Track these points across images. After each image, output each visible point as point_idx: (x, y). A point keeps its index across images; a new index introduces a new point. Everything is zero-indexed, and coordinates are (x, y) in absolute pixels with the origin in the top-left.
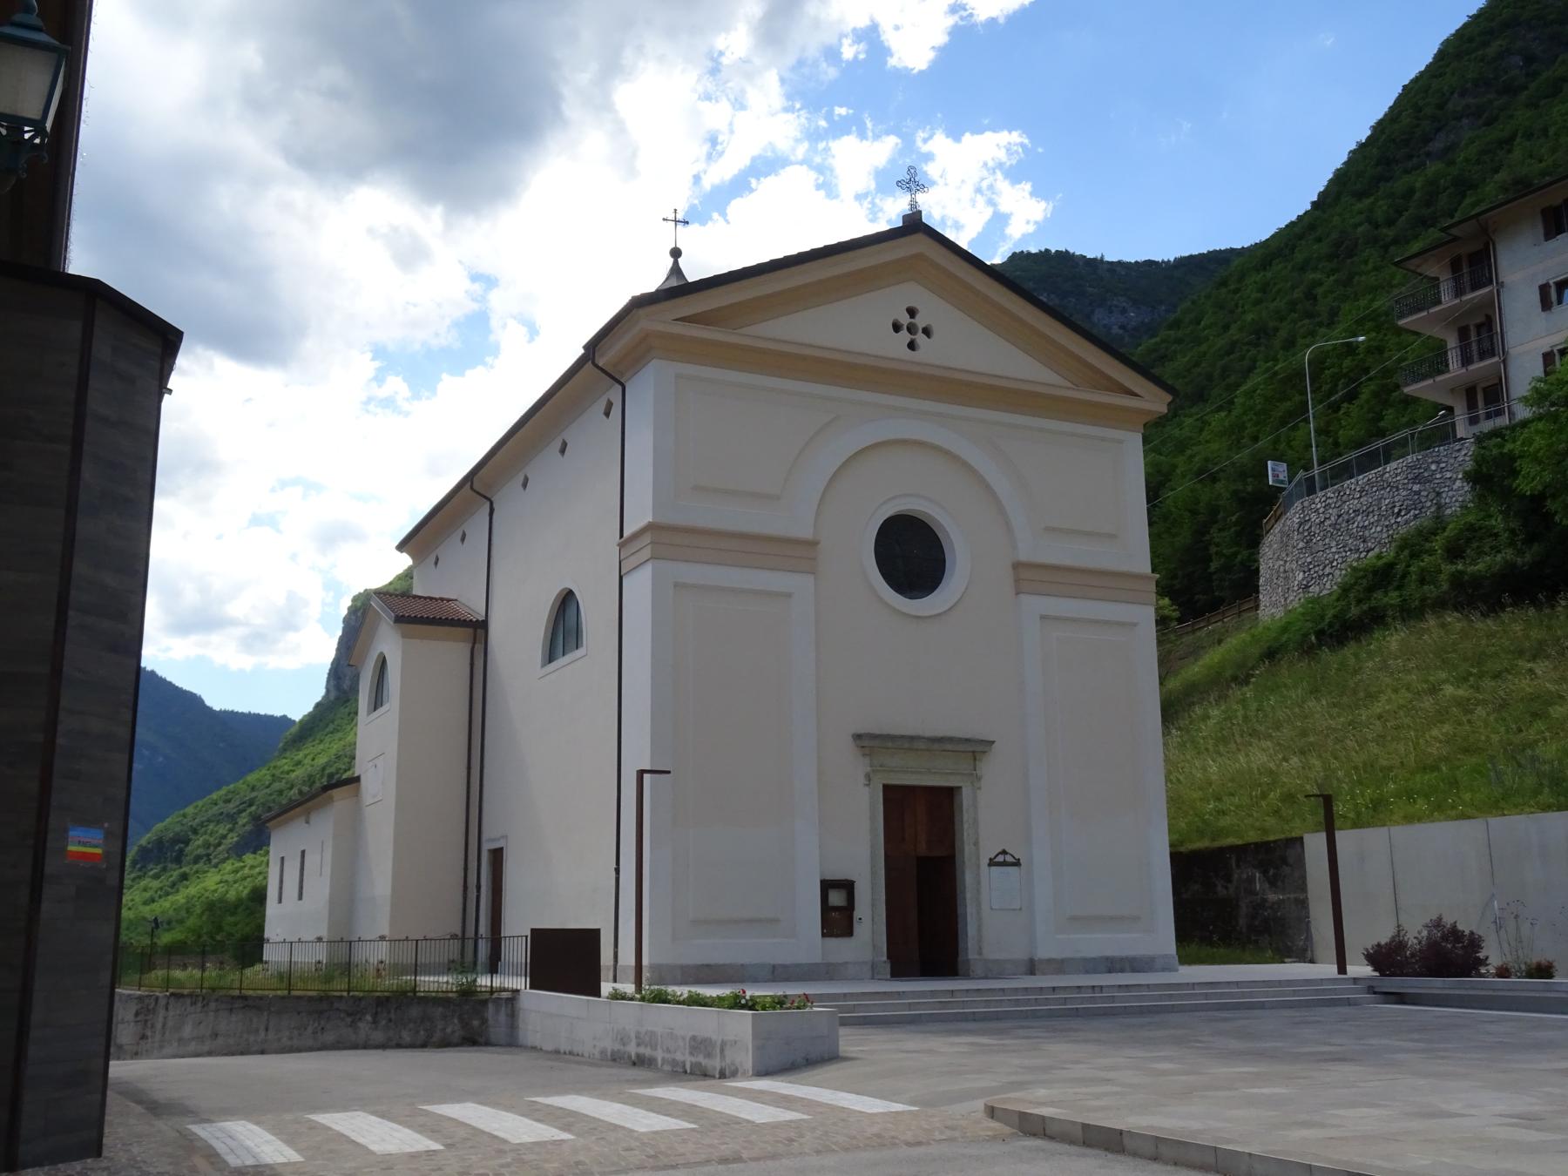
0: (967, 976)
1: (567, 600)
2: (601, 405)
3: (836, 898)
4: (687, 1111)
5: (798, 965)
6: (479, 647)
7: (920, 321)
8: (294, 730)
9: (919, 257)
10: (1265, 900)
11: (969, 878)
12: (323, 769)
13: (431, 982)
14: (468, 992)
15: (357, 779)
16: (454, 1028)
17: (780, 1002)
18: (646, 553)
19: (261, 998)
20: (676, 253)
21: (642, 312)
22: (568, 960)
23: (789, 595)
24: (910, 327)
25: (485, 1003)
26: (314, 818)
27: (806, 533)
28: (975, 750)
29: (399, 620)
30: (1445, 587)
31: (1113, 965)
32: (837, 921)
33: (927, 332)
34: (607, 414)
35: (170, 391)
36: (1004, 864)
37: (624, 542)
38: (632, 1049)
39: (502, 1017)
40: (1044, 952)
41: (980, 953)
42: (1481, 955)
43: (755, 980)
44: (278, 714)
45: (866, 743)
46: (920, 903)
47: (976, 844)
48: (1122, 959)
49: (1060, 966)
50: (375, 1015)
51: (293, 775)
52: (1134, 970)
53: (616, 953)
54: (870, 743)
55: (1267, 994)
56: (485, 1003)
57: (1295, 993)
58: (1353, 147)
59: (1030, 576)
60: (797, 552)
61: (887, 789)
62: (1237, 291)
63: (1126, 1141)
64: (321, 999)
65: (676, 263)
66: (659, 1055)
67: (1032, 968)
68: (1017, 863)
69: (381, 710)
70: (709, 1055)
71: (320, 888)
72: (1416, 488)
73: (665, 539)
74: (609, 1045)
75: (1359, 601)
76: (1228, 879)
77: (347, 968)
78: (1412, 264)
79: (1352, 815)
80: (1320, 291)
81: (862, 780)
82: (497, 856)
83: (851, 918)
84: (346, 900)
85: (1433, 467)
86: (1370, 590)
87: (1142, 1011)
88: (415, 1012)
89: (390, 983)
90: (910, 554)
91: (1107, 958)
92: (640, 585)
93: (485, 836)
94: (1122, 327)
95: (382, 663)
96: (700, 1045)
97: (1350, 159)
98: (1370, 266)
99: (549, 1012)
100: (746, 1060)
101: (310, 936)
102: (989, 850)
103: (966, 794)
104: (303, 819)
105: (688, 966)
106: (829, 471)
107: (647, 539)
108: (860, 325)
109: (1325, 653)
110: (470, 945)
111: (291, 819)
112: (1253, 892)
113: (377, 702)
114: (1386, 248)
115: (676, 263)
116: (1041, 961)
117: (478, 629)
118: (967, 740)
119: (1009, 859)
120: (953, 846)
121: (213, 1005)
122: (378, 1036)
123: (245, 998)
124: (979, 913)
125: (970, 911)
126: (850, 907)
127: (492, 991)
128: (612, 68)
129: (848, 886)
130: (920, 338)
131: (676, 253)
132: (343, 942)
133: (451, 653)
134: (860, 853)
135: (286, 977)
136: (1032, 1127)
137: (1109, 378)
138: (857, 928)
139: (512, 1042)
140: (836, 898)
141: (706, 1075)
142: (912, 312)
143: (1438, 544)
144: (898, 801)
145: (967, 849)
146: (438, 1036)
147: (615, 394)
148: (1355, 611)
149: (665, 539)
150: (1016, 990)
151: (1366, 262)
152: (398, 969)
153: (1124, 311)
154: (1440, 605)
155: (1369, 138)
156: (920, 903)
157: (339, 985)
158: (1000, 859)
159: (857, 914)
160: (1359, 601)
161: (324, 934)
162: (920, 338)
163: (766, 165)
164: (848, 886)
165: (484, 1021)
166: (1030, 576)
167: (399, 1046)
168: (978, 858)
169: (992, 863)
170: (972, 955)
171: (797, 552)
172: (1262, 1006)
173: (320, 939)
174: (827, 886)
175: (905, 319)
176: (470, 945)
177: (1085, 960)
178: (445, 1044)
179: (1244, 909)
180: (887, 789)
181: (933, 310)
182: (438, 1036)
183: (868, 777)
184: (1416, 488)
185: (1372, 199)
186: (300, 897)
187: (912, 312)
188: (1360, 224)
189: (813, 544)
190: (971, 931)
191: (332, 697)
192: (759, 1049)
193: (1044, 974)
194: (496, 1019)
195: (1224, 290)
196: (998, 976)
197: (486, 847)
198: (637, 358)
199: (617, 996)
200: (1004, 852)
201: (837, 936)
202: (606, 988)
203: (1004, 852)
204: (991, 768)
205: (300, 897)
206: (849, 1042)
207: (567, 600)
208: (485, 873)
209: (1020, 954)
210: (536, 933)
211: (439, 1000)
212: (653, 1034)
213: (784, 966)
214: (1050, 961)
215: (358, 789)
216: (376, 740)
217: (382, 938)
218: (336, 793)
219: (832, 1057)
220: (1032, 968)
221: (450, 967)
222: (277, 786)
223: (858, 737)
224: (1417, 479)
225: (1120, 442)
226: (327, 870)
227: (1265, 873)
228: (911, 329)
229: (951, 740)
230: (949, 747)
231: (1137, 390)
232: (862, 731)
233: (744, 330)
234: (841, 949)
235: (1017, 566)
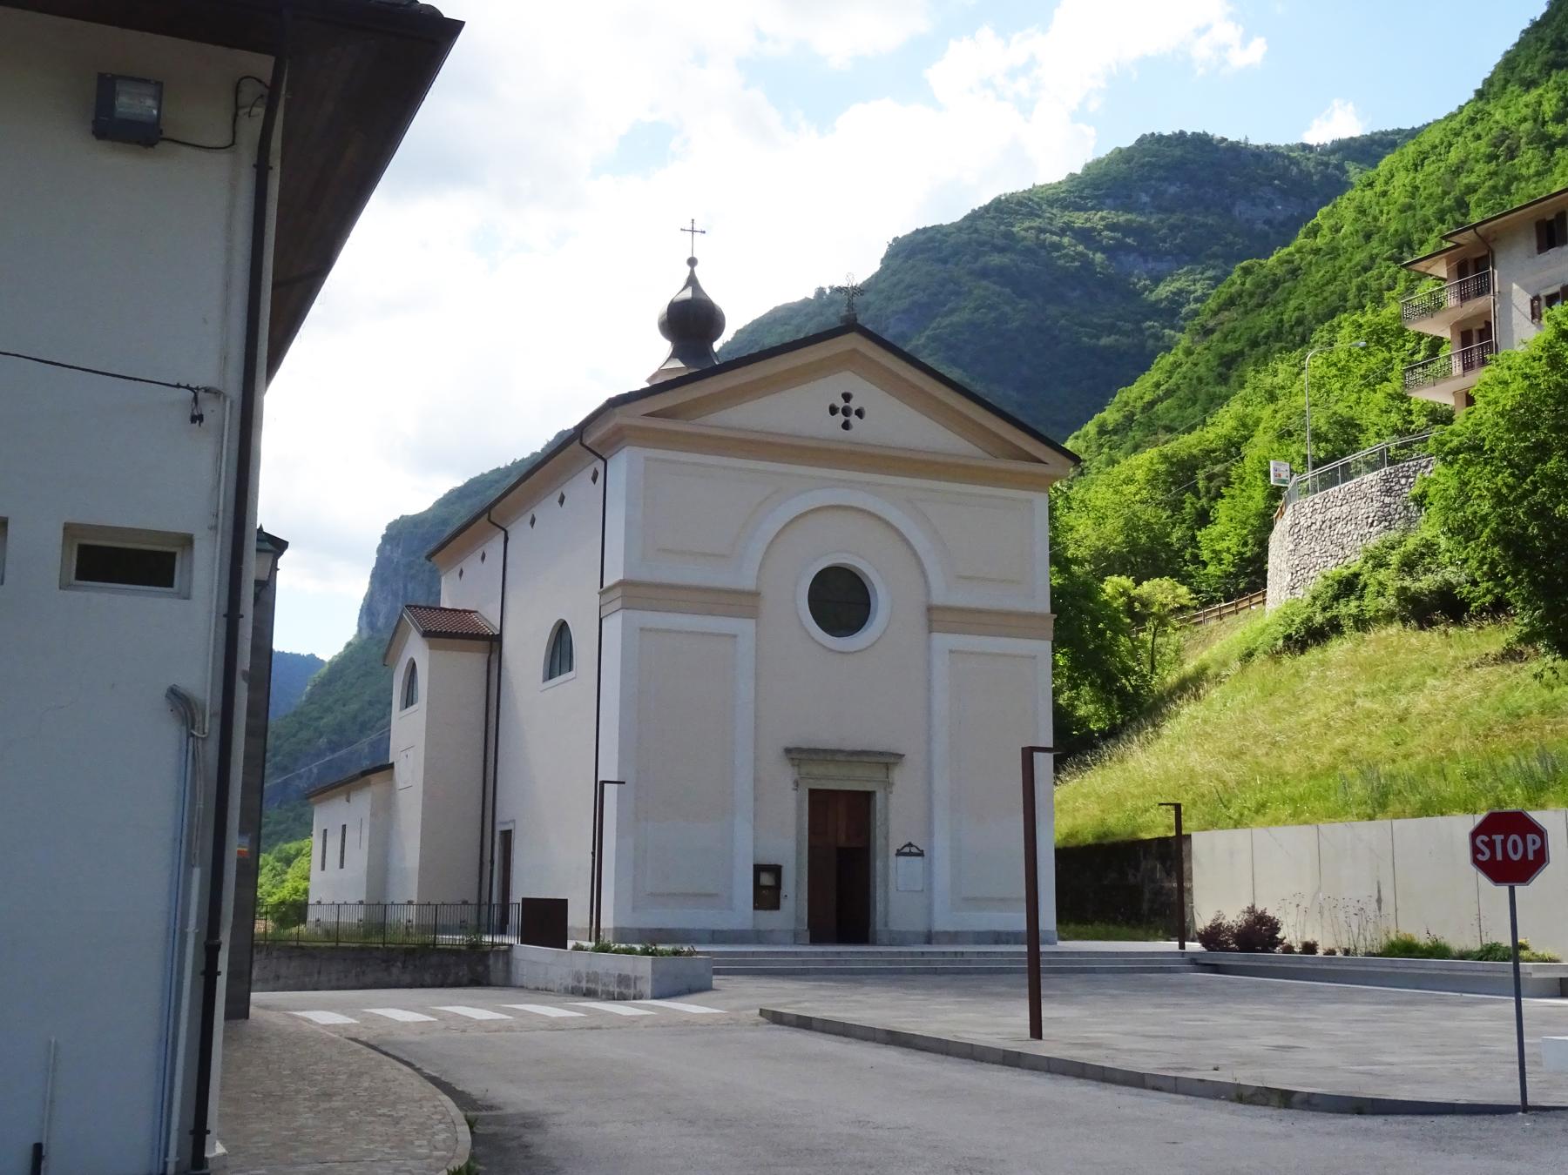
0: (874, 943)
1: (562, 630)
2: (589, 473)
3: (766, 879)
4: (587, 1010)
6: (494, 657)
7: (854, 405)
8: (324, 670)
9: (854, 351)
11: (879, 864)
12: (355, 717)
13: (445, 939)
14: (474, 947)
15: (392, 766)
16: (464, 971)
17: (676, 953)
18: (618, 604)
19: (315, 948)
20: (692, 262)
21: (617, 410)
22: (546, 922)
24: (846, 411)
25: (486, 954)
26: (353, 798)
27: (748, 583)
28: (888, 760)
29: (426, 634)
30: (1393, 601)
32: (767, 895)
33: (860, 413)
34: (594, 479)
36: (910, 854)
37: (604, 591)
38: (584, 985)
39: (500, 965)
40: (942, 924)
41: (886, 924)
42: (1279, 936)
43: (699, 942)
44: (305, 652)
46: (837, 886)
47: (886, 838)
48: (1008, 934)
49: (954, 937)
50: (404, 963)
51: (322, 723)
53: (577, 917)
54: (798, 755)
55: (1101, 962)
56: (486, 954)
58: (1527, 25)
60: (744, 602)
61: (812, 792)
62: (1384, 194)
63: (814, 1024)
64: (362, 949)
65: (692, 272)
66: (600, 988)
67: (929, 938)
68: (921, 854)
69: (411, 708)
70: (628, 986)
71: (358, 857)
72: (1387, 500)
73: (632, 594)
74: (570, 983)
75: (1324, 609)
76: (1137, 869)
77: (382, 928)
78: (1421, 267)
79: (1236, 816)
80: (1472, 199)
81: (791, 785)
82: (507, 836)
84: (380, 871)
85: (1403, 481)
86: (1336, 598)
87: (990, 971)
88: (434, 960)
89: (416, 939)
90: (840, 601)
92: (613, 625)
93: (498, 819)
94: (1268, 222)
95: (412, 668)
96: (623, 980)
97: (1521, 39)
98: (1532, 171)
99: (531, 957)
100: (647, 988)
101: (352, 899)
102: (897, 842)
103: (879, 796)
104: (344, 797)
106: (777, 527)
107: (618, 592)
109: (1286, 660)
110: (485, 909)
111: (333, 797)
113: (409, 701)
114: (1551, 148)
115: (692, 272)
117: (494, 642)
118: (881, 754)
119: (914, 850)
120: (868, 840)
121: (275, 954)
122: (407, 978)
123: (302, 948)
124: (886, 893)
125: (879, 893)
126: (777, 887)
127: (493, 944)
129: (776, 870)
130: (853, 419)
131: (692, 262)
132: (377, 906)
133: (471, 662)
134: (787, 843)
135: (333, 933)
136: (777, 1018)
137: (1016, 447)
138: (783, 902)
139: (507, 982)
140: (766, 879)
141: (625, 998)
142: (847, 397)
143: (1394, 559)
144: (821, 803)
145: (879, 842)
146: (451, 979)
147: (599, 465)
148: (1319, 619)
149: (632, 594)
150: (912, 954)
151: (1528, 166)
152: (423, 929)
153: (1269, 204)
154: (1390, 617)
155: (1544, 16)
156: (837, 886)
157: (376, 941)
158: (907, 850)
159: (783, 892)
160: (1324, 609)
161: (415, 900)
162: (853, 419)
164: (776, 870)
165: (487, 967)
167: (422, 986)
169: (899, 853)
170: (879, 926)
171: (744, 602)
172: (1093, 971)
173: (361, 903)
174: (759, 869)
175: (840, 404)
176: (485, 909)
177: (979, 933)
178: (457, 984)
179: (1147, 896)
182: (451, 979)
183: (797, 784)
184: (1387, 500)
185: (1540, 91)
186: (342, 866)
187: (847, 397)
188: (1525, 120)
189: (756, 594)
190: (880, 907)
191: (365, 636)
192: (655, 981)
194: (496, 966)
195: (1369, 193)
196: (901, 944)
197: (499, 828)
198: (617, 439)
199: (578, 948)
200: (910, 845)
202: (570, 944)
203: (910, 845)
204: (897, 775)
205: (342, 866)
206: (717, 981)
207: (562, 630)
208: (496, 848)
209: (920, 927)
210: (524, 900)
211: (454, 952)
212: (596, 973)
213: (722, 932)
215: (391, 778)
216: (408, 734)
217: (410, 903)
218: (373, 778)
219: (706, 988)
220: (929, 938)
221: (462, 928)
222: (304, 735)
223: (788, 751)
224: (1388, 492)
226: (365, 844)
227: (1163, 863)
228: (846, 412)
232: (791, 746)
234: (769, 919)
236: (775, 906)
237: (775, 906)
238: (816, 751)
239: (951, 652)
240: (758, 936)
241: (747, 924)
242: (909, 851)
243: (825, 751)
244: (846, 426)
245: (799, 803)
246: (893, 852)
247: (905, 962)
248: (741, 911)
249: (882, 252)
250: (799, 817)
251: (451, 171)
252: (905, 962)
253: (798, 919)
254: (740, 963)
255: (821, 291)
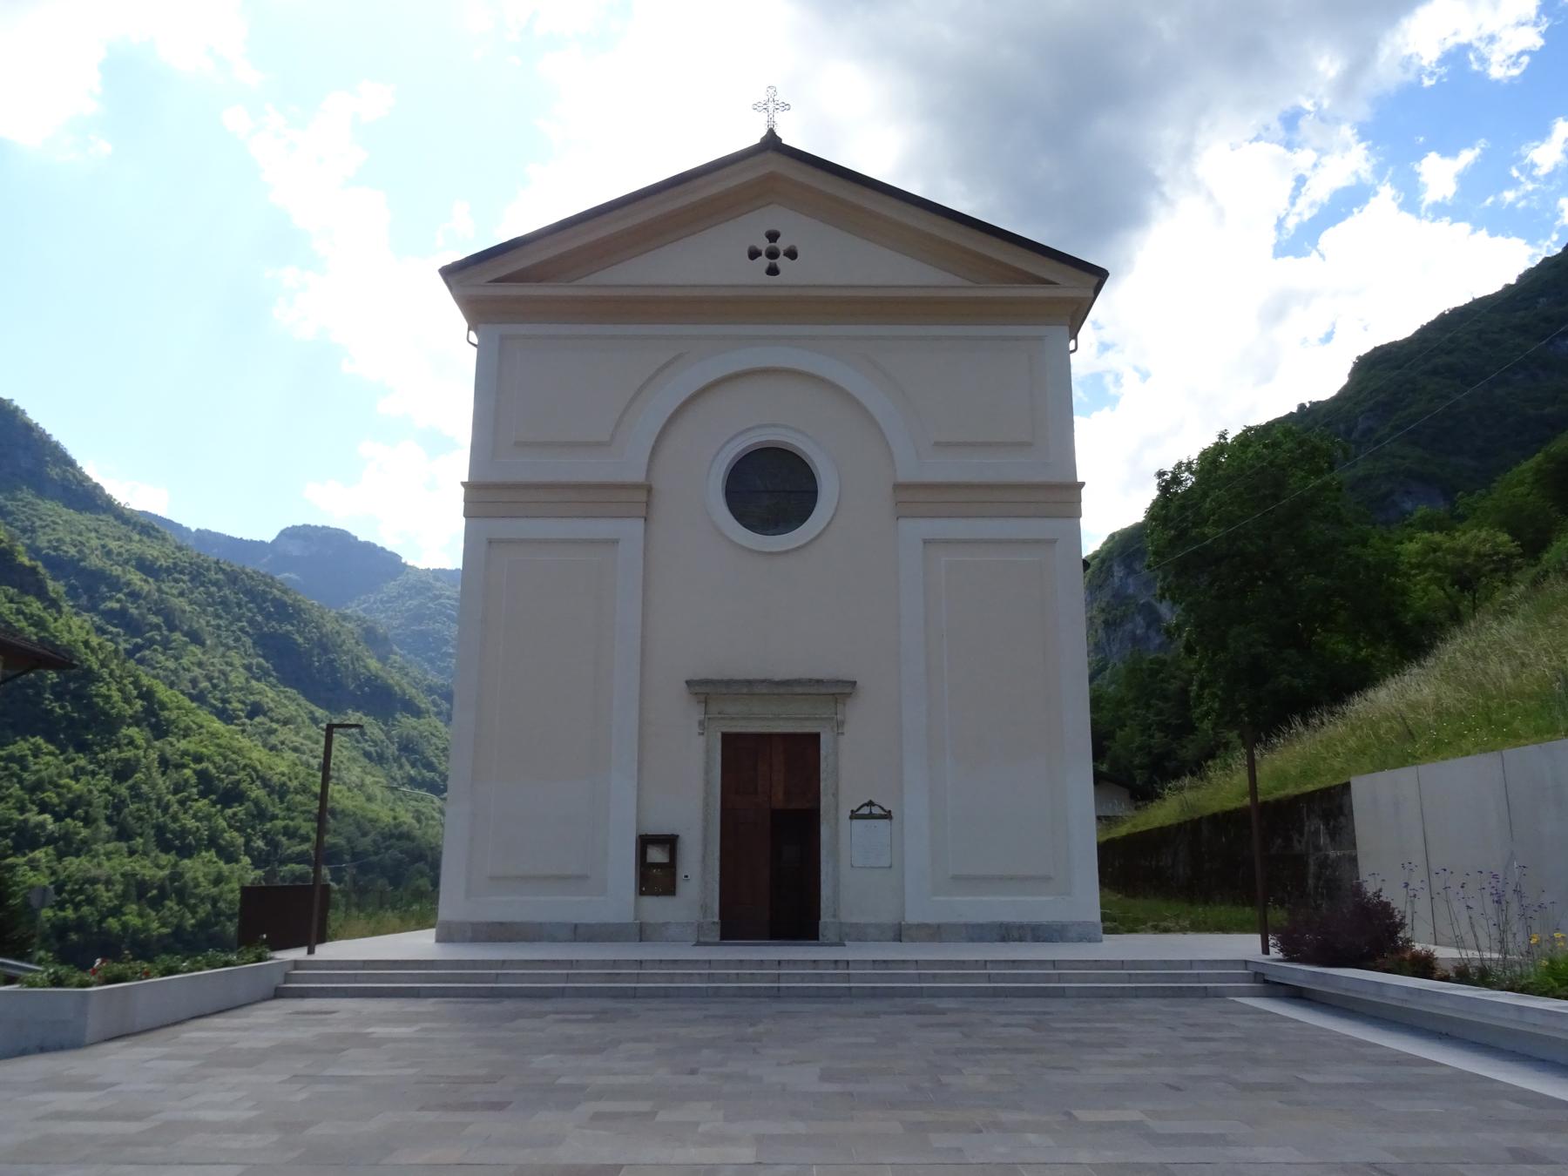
3: (657, 855)
5: (605, 925)
9: (772, 177)
10: (1327, 857)
23: (615, 542)
24: (773, 253)
28: (839, 691)
31: (1006, 933)
32: (656, 877)
33: (792, 254)
35: (1083, 484)
36: (871, 816)
40: (912, 918)
45: (698, 689)
47: (835, 795)
48: (1021, 927)
49: (936, 933)
52: (1037, 939)
54: (705, 691)
57: (1130, 978)
59: (914, 497)
68: (887, 816)
81: (696, 729)
83: (674, 875)
90: (771, 489)
91: (1001, 925)
105: (478, 924)
108: (716, 259)
112: (1317, 848)
116: (910, 926)
119: (876, 810)
126: (671, 867)
128: (1186, 153)
129: (670, 842)
134: (690, 806)
138: (682, 886)
140: (657, 855)
144: (741, 755)
158: (866, 811)
163: (1349, 201)
166: (914, 497)
168: (837, 808)
169: (854, 815)
174: (645, 842)
179: (1312, 868)
180: (729, 740)
181: (795, 228)
187: (773, 236)
193: (913, 940)
201: (658, 894)
203: (871, 804)
214: (919, 926)
220: (899, 933)
225: (1040, 338)
228: (773, 254)
229: (799, 682)
230: (799, 690)
231: (1051, 278)
233: (583, 281)
234: (657, 908)
235: (898, 487)
236: (669, 889)
237: (669, 889)
238: (729, 683)
239: (926, 542)
240: (642, 933)
241: (628, 917)
242: (869, 812)
243: (749, 683)
244: (773, 271)
245: (708, 751)
246: (845, 814)
247: (727, 978)
248: (617, 895)
249: (1349, 367)
250: (707, 771)
251: (1104, 398)
252: (727, 978)
253: (704, 908)
254: (429, 978)
255: (1302, 406)
